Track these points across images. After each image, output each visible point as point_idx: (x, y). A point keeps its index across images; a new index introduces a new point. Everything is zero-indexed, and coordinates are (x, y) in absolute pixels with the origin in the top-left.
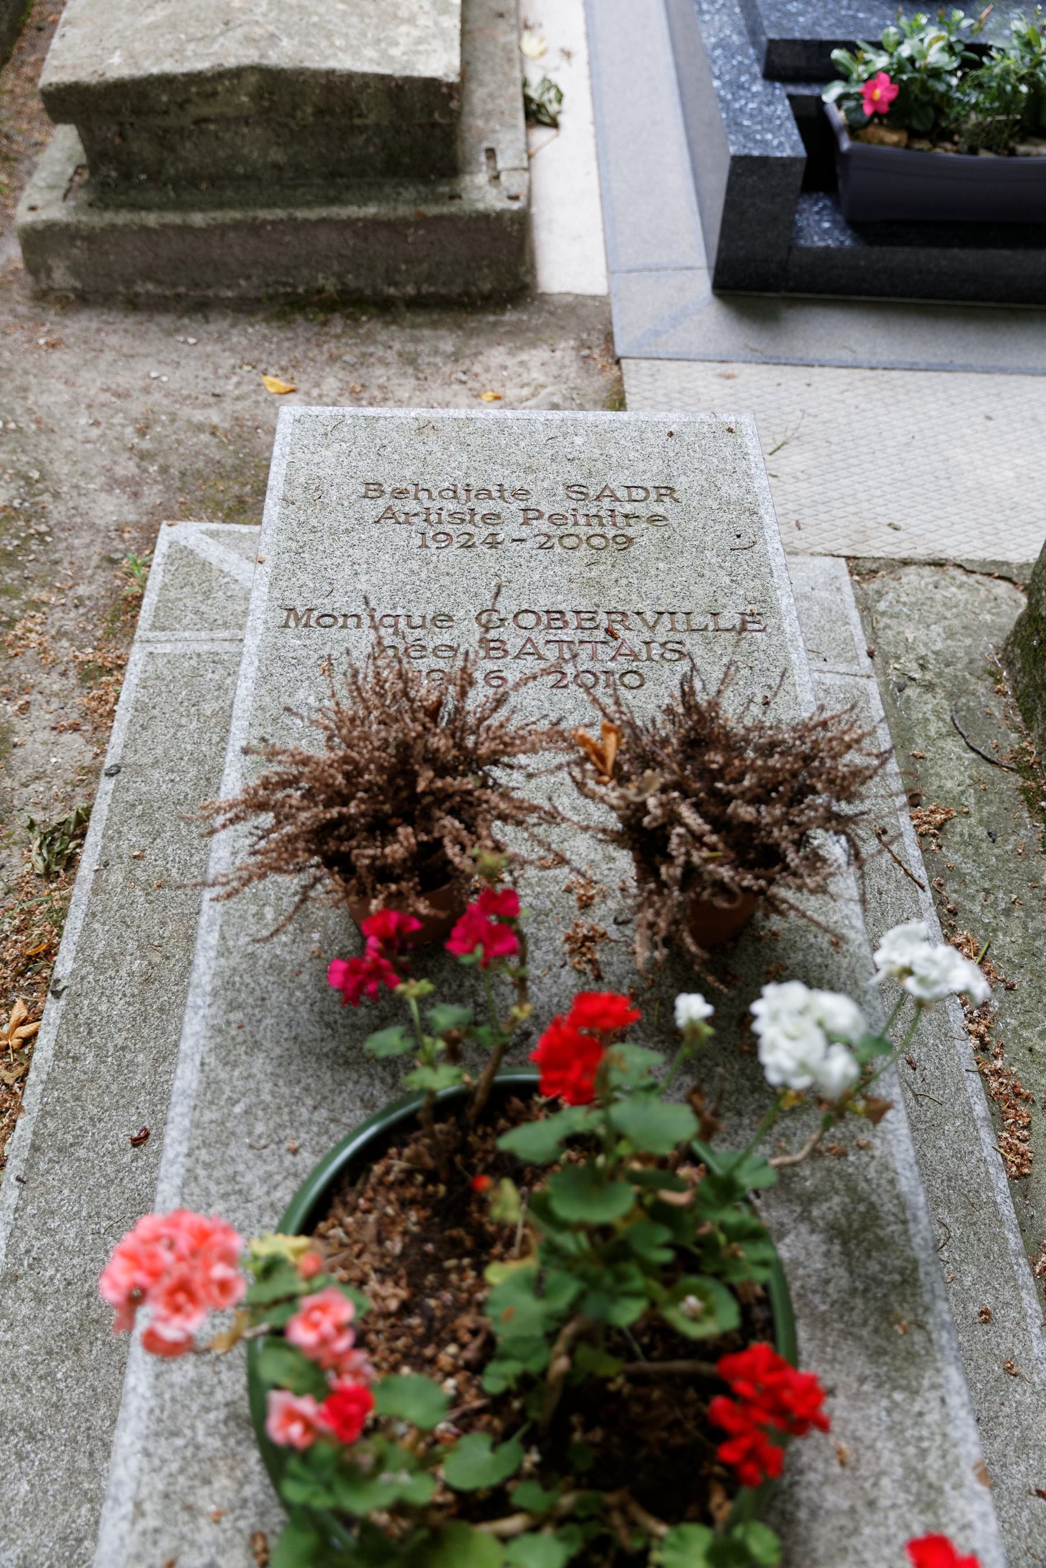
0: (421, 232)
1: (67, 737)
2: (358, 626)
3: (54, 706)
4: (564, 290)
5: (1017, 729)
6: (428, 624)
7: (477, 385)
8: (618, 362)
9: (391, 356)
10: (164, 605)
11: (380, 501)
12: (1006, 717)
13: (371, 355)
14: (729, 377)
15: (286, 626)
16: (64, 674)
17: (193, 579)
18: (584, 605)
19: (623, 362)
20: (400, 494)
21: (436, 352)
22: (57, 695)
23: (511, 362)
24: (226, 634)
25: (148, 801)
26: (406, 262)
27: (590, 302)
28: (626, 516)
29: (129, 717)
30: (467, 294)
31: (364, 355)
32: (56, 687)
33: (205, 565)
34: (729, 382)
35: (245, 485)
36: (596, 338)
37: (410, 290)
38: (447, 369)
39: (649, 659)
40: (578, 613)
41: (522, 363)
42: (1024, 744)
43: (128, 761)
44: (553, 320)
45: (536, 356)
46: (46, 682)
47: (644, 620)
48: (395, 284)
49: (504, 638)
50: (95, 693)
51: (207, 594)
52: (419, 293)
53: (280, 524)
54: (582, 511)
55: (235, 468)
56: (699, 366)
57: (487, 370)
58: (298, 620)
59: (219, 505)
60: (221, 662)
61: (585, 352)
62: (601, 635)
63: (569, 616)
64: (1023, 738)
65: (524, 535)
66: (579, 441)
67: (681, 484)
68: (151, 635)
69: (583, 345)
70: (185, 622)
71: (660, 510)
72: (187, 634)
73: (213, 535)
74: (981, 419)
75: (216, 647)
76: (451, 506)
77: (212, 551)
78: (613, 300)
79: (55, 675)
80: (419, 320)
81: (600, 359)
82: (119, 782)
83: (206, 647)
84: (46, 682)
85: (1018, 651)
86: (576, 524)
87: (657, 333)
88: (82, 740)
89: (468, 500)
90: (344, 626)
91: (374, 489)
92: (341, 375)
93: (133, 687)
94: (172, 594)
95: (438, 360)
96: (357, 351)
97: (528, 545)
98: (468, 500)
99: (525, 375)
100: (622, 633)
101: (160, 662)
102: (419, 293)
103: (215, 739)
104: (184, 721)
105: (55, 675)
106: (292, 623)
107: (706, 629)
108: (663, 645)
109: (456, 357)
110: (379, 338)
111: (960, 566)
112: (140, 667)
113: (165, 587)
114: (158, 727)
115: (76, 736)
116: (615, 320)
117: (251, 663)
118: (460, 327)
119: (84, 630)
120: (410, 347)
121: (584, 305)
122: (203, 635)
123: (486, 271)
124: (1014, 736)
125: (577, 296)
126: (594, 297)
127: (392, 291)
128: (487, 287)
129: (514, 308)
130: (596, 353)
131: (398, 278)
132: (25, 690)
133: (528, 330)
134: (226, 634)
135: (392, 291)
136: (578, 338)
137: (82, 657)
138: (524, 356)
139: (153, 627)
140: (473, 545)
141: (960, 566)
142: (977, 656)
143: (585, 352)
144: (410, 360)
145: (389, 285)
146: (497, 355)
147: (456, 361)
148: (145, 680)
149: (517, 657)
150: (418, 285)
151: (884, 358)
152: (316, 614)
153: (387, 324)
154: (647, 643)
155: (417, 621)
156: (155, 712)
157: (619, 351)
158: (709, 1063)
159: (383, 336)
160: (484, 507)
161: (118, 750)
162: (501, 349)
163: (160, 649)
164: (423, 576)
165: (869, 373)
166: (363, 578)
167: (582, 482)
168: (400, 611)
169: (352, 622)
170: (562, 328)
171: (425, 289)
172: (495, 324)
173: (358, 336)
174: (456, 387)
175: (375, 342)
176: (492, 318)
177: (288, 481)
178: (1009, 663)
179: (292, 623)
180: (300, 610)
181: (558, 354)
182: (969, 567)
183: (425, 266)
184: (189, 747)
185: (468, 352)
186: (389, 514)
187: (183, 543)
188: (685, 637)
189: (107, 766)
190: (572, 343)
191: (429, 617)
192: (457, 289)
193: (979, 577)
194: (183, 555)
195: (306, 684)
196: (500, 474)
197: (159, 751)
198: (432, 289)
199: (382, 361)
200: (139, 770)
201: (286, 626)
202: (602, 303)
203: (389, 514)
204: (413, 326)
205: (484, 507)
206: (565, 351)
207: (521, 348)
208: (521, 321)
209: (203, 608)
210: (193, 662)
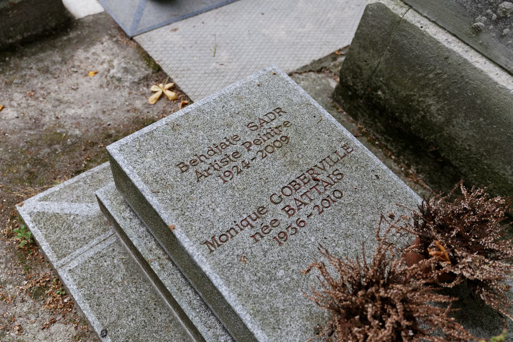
0: (15, 11)
1: (53, 328)
2: (237, 233)
3: (33, 319)
4: (86, 14)
5: (353, 122)
6: (259, 215)
7: (83, 71)
8: (131, 39)
9: (34, 72)
10: (55, 245)
11: (191, 171)
12: (348, 120)
13: (25, 75)
14: (175, 30)
15: (212, 251)
16: (23, 301)
17: (56, 225)
18: (297, 173)
19: (134, 38)
20: (194, 163)
21: (54, 63)
22: (29, 313)
23: (89, 55)
24: (95, 242)
25: (131, 335)
26: (12, 26)
27: (100, 16)
28: (276, 128)
29: (88, 305)
30: (46, 30)
31: (22, 77)
32: (25, 309)
33: (56, 216)
34: (177, 32)
35: (25, 164)
36: (115, 32)
37: (19, 37)
38: (64, 68)
39: (335, 182)
40: (298, 178)
41: (94, 54)
42: (359, 126)
43: (106, 324)
44: (92, 30)
45: (98, 48)
46: (18, 310)
47: (319, 168)
48: (11, 37)
49: (287, 204)
50: (50, 299)
51: (69, 228)
52: (23, 37)
53: (163, 205)
54: (262, 134)
55: (13, 158)
56: (162, 29)
57: (81, 62)
58: (213, 245)
59: (21, 180)
60: (105, 255)
61: (115, 39)
62: (314, 183)
63: (298, 181)
64: (357, 124)
65: (253, 156)
66: (232, 103)
67: (280, 104)
68: (62, 262)
69: (112, 36)
70: (72, 246)
71: (283, 119)
72: (78, 252)
73: (45, 199)
74: (261, 15)
75: (97, 249)
76: (218, 158)
77: (53, 207)
78: (109, 12)
79: (19, 304)
80: (33, 50)
81: (125, 41)
82: (111, 336)
83: (92, 253)
84: (18, 310)
85: (341, 97)
86: (265, 141)
87: (138, 21)
88: (62, 326)
89: (221, 151)
90: (232, 236)
91: (183, 167)
92: (19, 90)
93: (76, 291)
94: (53, 237)
95: (58, 66)
96: (18, 76)
97: (258, 159)
98: (221, 151)
99: (99, 59)
100: (318, 177)
101: (78, 271)
102: (23, 37)
103: (134, 290)
104: (113, 291)
105: (19, 304)
106: (213, 249)
107: (338, 160)
108: (333, 174)
109: (64, 61)
110: (22, 66)
111: (296, 73)
112: (71, 280)
113: (46, 236)
114: (105, 300)
115: (56, 325)
116: (117, 21)
117: (216, 278)
118: (55, 47)
119: (12, 275)
120: (41, 65)
121: (100, 19)
122: (85, 247)
123: (50, 18)
124: (354, 124)
125: (93, 15)
126: (101, 14)
127: (10, 41)
128: (53, 24)
129: (71, 30)
130: (119, 37)
131: (11, 34)
132: (12, 320)
133: (85, 38)
134: (95, 242)
135: (10, 41)
136: (108, 34)
137: (25, 288)
138: (93, 50)
139: (59, 258)
140: (241, 171)
141: (296, 73)
142: (326, 103)
143: (115, 39)
144: (46, 71)
145: (8, 39)
146: (80, 54)
147: (66, 63)
148: (79, 284)
149: (299, 209)
150: (21, 34)
151: (217, 3)
152: (217, 238)
153: (21, 57)
154: (328, 177)
155: (254, 216)
156: (97, 295)
157: (130, 34)
158: (478, 318)
159: (24, 64)
160: (229, 151)
161: (97, 322)
162: (80, 50)
163: (74, 264)
164: (237, 195)
165: (217, 11)
166: (218, 210)
167: (250, 121)
168: (245, 216)
169: (232, 232)
170: (98, 32)
171: (25, 35)
172: (69, 40)
173: (11, 69)
174: (75, 75)
175: (22, 69)
176: (65, 38)
177: (146, 183)
178: (338, 101)
179: (213, 249)
180: (210, 240)
181: (105, 44)
182: (299, 72)
183: (22, 25)
184: (126, 301)
185: (67, 57)
186: (199, 176)
187: (35, 211)
188: (335, 167)
189: (99, 333)
190: (107, 37)
191: (256, 212)
192: (41, 30)
193: (305, 74)
194: (40, 217)
195: (244, 272)
196: (221, 134)
197: (115, 310)
198: (29, 34)
199: (32, 76)
200: (115, 325)
201: (212, 251)
202: (105, 14)
203: (199, 176)
204: (34, 54)
205: (229, 151)
206: (107, 43)
207: (88, 47)
208: (79, 35)
209: (74, 236)
210: (93, 262)
